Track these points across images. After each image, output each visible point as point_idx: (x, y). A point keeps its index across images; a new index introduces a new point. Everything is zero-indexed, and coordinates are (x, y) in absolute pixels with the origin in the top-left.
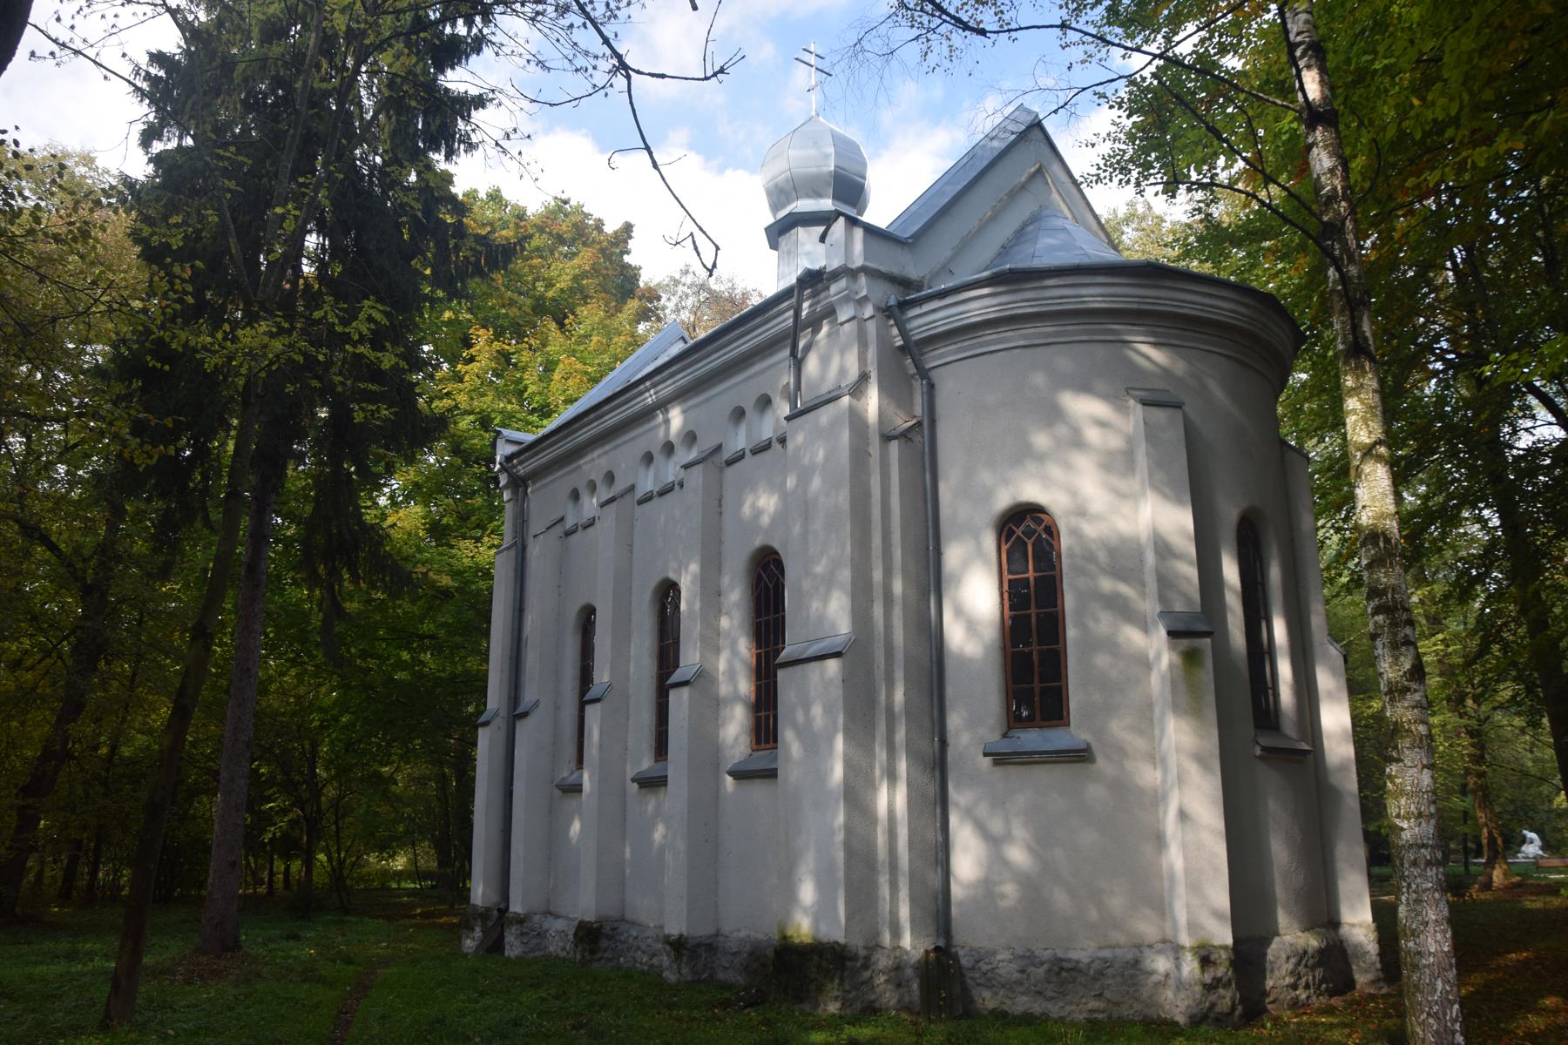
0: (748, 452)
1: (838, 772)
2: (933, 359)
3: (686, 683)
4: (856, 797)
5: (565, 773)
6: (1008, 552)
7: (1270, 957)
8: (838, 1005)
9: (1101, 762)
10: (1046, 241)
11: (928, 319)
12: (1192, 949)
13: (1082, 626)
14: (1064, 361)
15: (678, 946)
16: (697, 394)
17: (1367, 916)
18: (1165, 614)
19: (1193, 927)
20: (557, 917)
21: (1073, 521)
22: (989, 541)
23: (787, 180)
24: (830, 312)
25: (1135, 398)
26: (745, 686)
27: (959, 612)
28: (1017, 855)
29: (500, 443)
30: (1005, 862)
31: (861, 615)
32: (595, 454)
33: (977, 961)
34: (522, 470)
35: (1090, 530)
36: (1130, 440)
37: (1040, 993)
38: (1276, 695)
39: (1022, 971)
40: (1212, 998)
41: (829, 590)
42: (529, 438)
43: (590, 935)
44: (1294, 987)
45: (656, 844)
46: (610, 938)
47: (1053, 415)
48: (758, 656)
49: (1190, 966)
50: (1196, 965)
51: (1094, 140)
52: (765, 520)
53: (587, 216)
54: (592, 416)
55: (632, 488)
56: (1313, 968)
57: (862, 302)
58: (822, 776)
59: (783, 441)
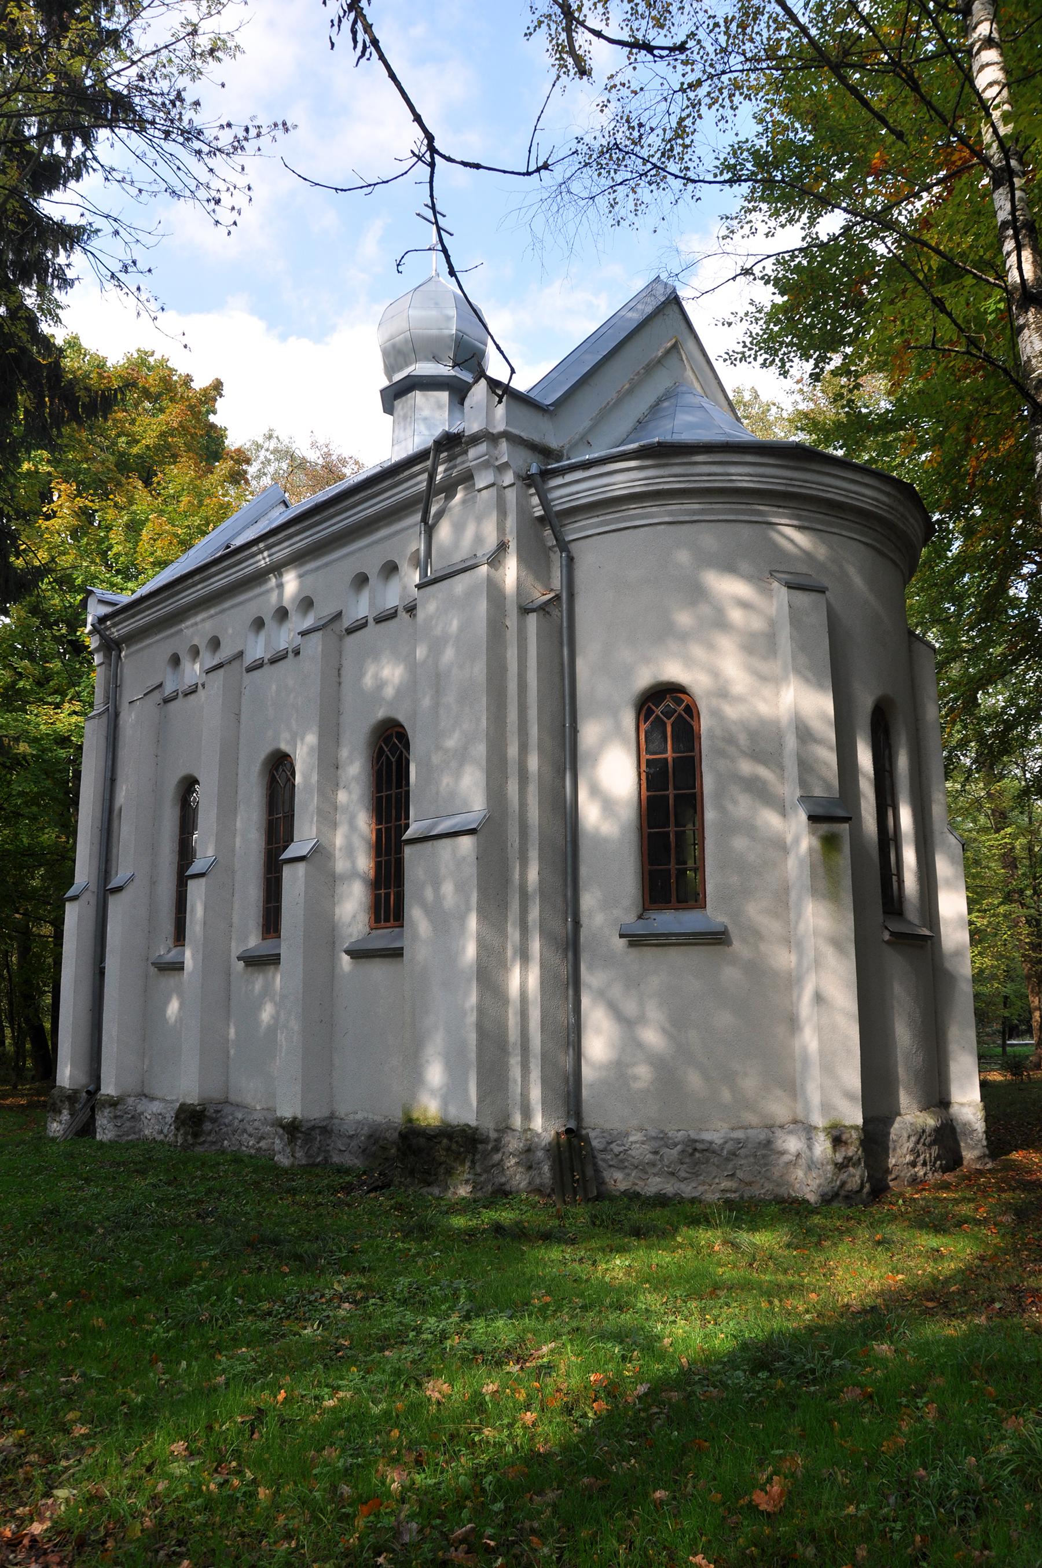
0: (371, 620)
1: (470, 951)
2: (573, 531)
3: (302, 859)
4: (489, 976)
5: (164, 951)
6: (646, 732)
7: (892, 1136)
8: (469, 1188)
9: (737, 945)
10: (684, 418)
11: (568, 491)
12: (825, 1129)
13: (721, 809)
14: (708, 538)
15: (292, 1129)
16: (315, 558)
17: (975, 1095)
18: (805, 799)
19: (826, 1107)
20: (153, 1099)
21: (715, 702)
22: (628, 719)
23: (406, 341)
24: (467, 478)
25: (779, 580)
26: (364, 863)
27: (595, 791)
28: (652, 1037)
29: (92, 602)
30: (639, 1045)
31: (495, 793)
32: (199, 618)
34: (115, 633)
35: (731, 712)
36: (772, 623)
37: (673, 1174)
38: (901, 881)
40: (843, 1176)
41: (461, 764)
42: (125, 598)
43: (193, 1119)
44: (913, 1164)
45: (264, 1025)
46: (214, 1121)
47: (696, 594)
48: (379, 832)
49: (822, 1147)
50: (828, 1144)
51: (732, 319)
52: (389, 692)
53: (171, 370)
54: (197, 578)
55: (240, 655)
56: (930, 1146)
57: (502, 468)
58: (451, 956)
59: (411, 609)
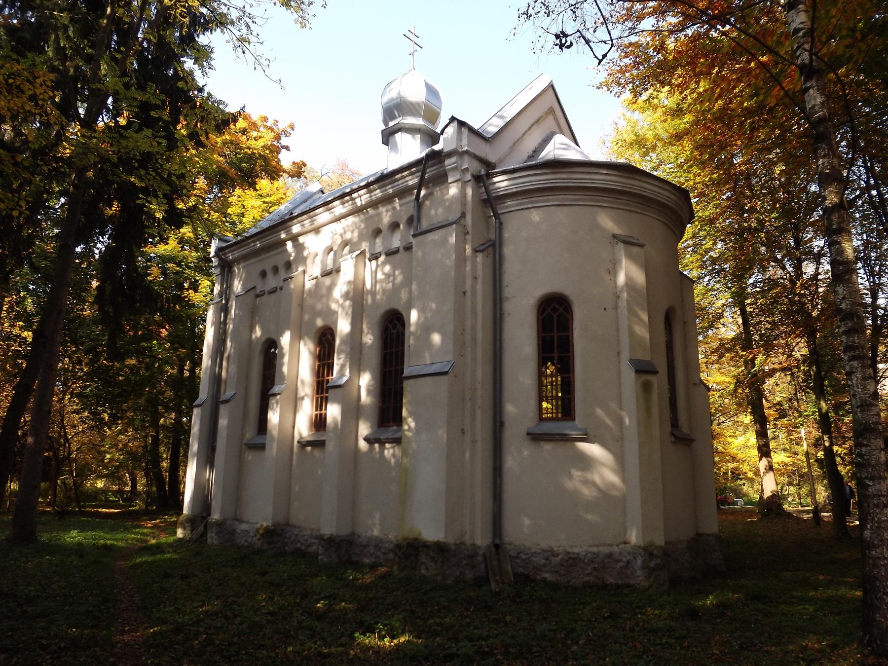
0: (401, 250)
15: (331, 542)
16: (255, 257)
20: (242, 522)
33: (519, 553)
37: (556, 572)
39: (547, 559)
43: (272, 534)
59: (281, 288)
